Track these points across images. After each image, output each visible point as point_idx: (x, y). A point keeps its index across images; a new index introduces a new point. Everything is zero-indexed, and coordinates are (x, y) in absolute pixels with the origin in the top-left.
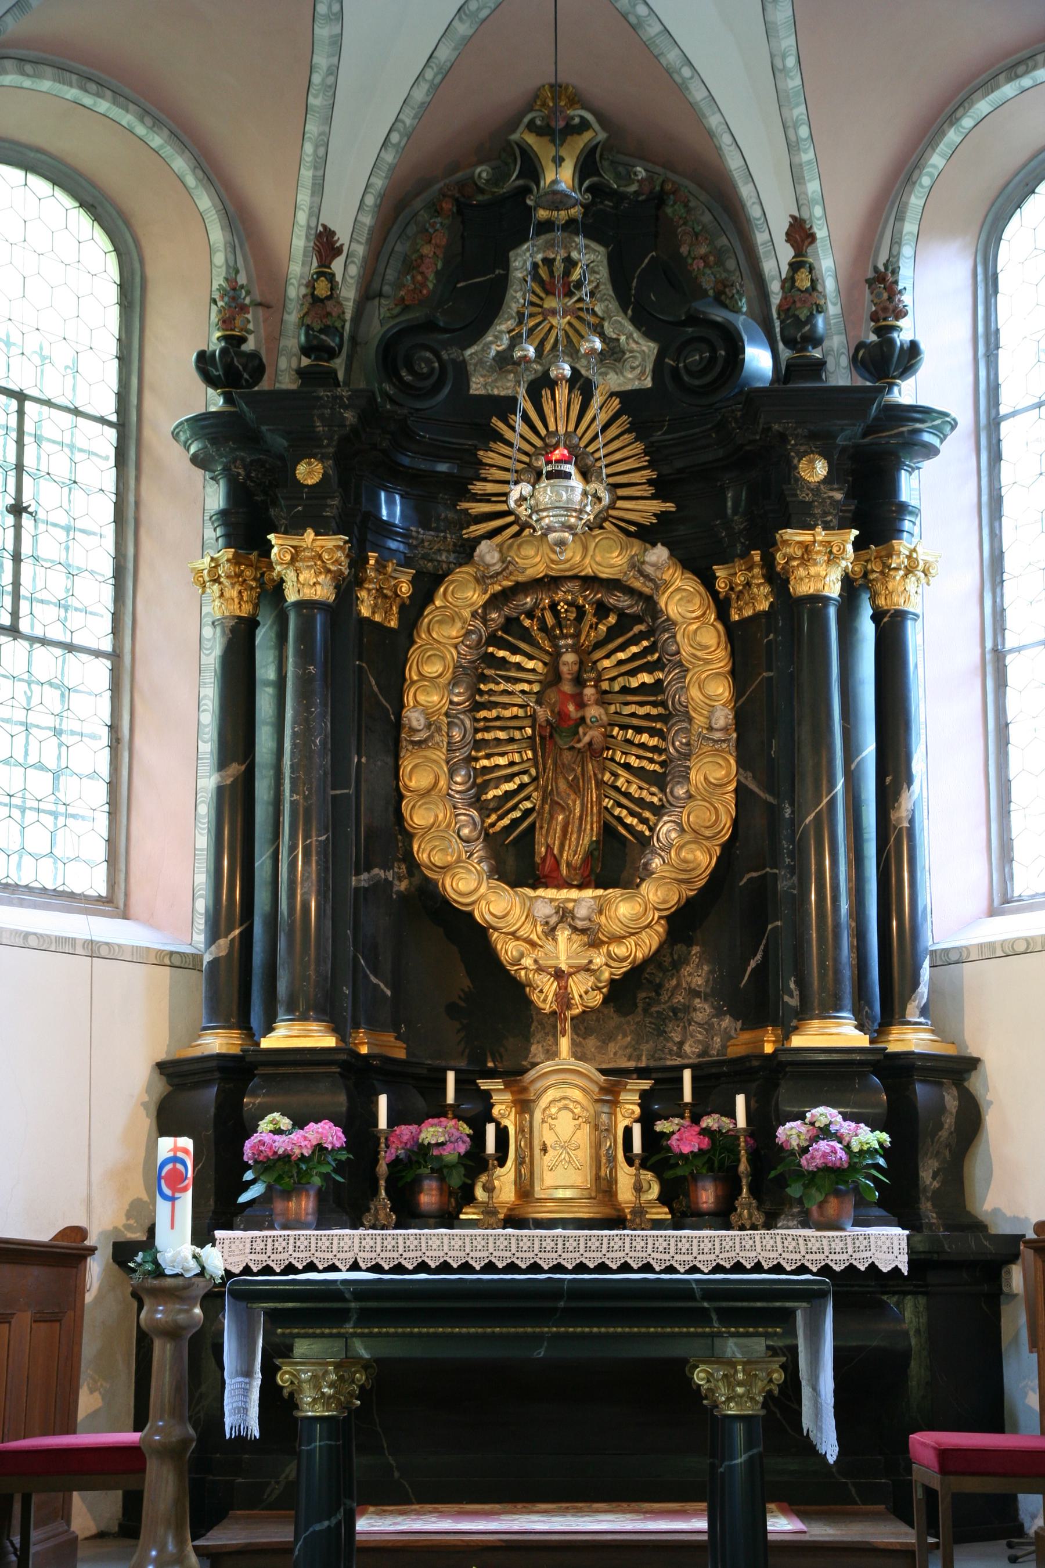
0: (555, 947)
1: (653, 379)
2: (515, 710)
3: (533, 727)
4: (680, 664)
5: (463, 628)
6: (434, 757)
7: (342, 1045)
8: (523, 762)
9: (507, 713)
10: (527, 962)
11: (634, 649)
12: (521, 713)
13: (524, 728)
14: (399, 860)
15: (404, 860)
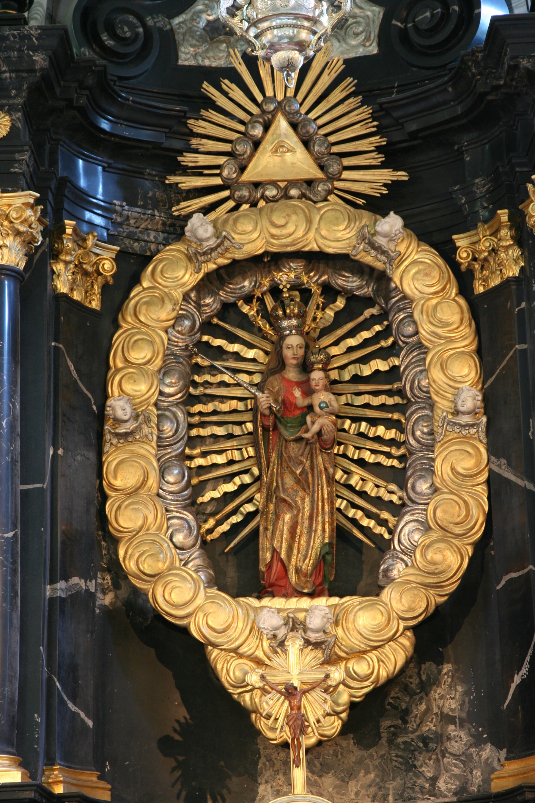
0: (286, 659)
1: (379, 45)
2: (234, 404)
3: (254, 422)
4: (420, 345)
5: (174, 310)
6: (142, 452)
7: (30, 781)
8: (243, 460)
9: (225, 407)
10: (254, 679)
11: (366, 335)
12: (240, 406)
13: (244, 422)
14: (103, 570)
15: (109, 570)
